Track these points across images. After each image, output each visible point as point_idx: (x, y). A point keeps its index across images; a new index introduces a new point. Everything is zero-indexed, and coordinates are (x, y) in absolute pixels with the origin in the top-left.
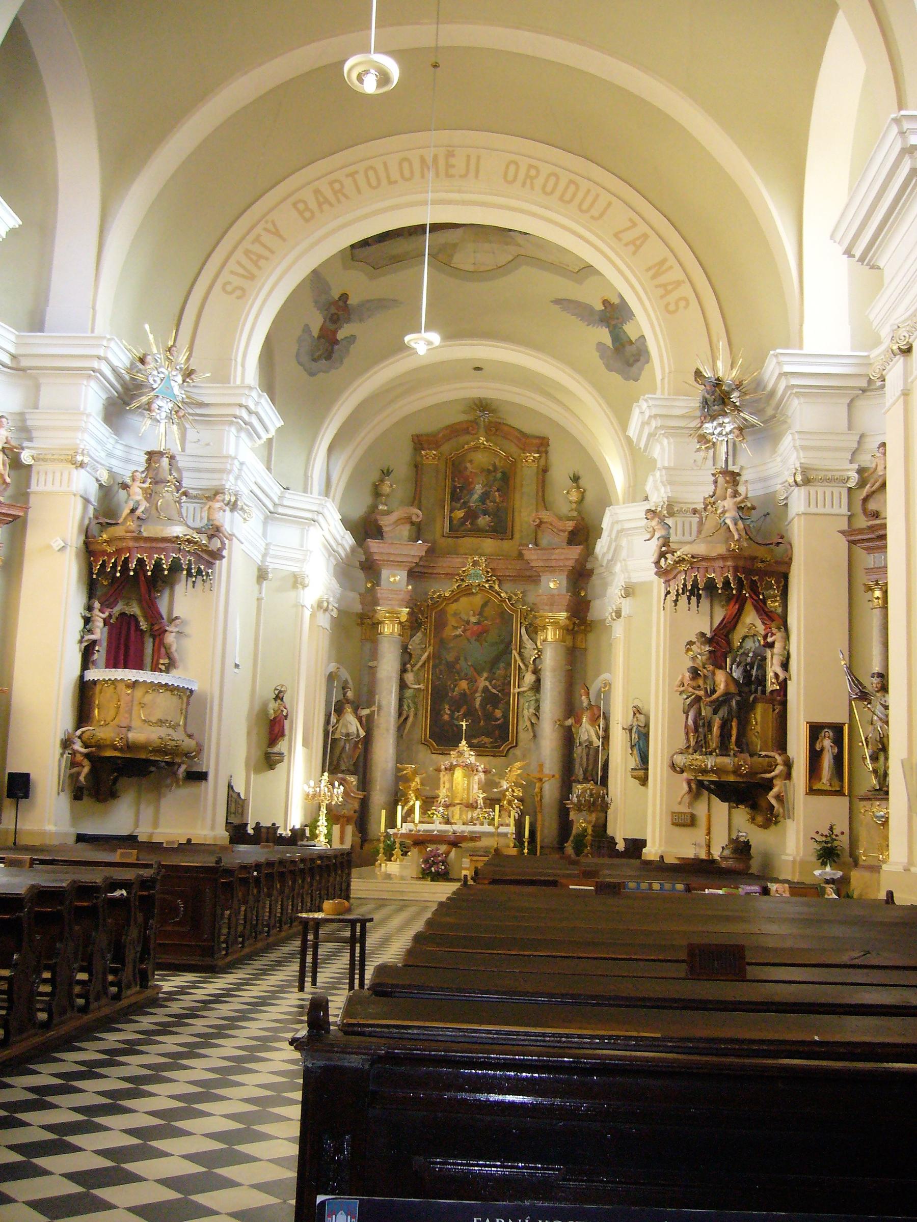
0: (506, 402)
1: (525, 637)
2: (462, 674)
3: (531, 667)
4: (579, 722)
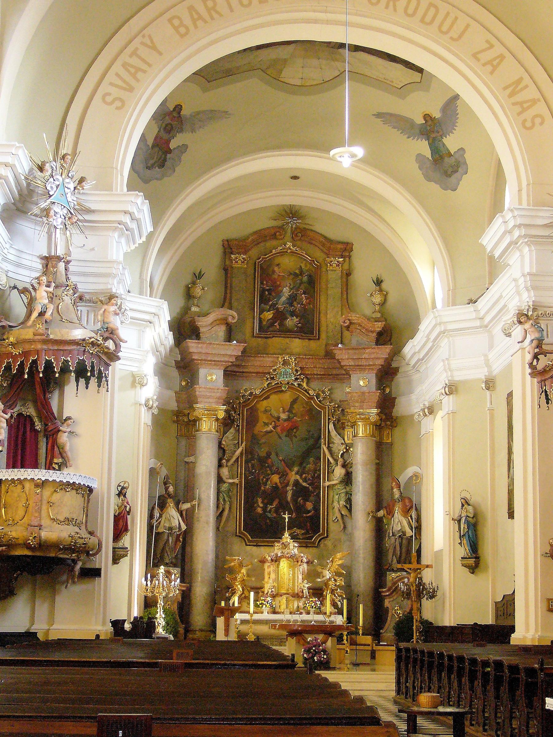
0: (314, 208)
1: (334, 433)
2: (274, 468)
3: (340, 461)
4: (391, 513)
